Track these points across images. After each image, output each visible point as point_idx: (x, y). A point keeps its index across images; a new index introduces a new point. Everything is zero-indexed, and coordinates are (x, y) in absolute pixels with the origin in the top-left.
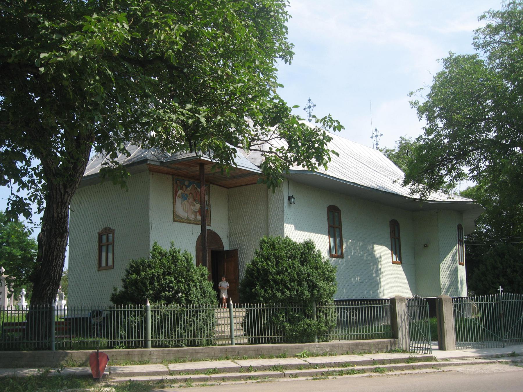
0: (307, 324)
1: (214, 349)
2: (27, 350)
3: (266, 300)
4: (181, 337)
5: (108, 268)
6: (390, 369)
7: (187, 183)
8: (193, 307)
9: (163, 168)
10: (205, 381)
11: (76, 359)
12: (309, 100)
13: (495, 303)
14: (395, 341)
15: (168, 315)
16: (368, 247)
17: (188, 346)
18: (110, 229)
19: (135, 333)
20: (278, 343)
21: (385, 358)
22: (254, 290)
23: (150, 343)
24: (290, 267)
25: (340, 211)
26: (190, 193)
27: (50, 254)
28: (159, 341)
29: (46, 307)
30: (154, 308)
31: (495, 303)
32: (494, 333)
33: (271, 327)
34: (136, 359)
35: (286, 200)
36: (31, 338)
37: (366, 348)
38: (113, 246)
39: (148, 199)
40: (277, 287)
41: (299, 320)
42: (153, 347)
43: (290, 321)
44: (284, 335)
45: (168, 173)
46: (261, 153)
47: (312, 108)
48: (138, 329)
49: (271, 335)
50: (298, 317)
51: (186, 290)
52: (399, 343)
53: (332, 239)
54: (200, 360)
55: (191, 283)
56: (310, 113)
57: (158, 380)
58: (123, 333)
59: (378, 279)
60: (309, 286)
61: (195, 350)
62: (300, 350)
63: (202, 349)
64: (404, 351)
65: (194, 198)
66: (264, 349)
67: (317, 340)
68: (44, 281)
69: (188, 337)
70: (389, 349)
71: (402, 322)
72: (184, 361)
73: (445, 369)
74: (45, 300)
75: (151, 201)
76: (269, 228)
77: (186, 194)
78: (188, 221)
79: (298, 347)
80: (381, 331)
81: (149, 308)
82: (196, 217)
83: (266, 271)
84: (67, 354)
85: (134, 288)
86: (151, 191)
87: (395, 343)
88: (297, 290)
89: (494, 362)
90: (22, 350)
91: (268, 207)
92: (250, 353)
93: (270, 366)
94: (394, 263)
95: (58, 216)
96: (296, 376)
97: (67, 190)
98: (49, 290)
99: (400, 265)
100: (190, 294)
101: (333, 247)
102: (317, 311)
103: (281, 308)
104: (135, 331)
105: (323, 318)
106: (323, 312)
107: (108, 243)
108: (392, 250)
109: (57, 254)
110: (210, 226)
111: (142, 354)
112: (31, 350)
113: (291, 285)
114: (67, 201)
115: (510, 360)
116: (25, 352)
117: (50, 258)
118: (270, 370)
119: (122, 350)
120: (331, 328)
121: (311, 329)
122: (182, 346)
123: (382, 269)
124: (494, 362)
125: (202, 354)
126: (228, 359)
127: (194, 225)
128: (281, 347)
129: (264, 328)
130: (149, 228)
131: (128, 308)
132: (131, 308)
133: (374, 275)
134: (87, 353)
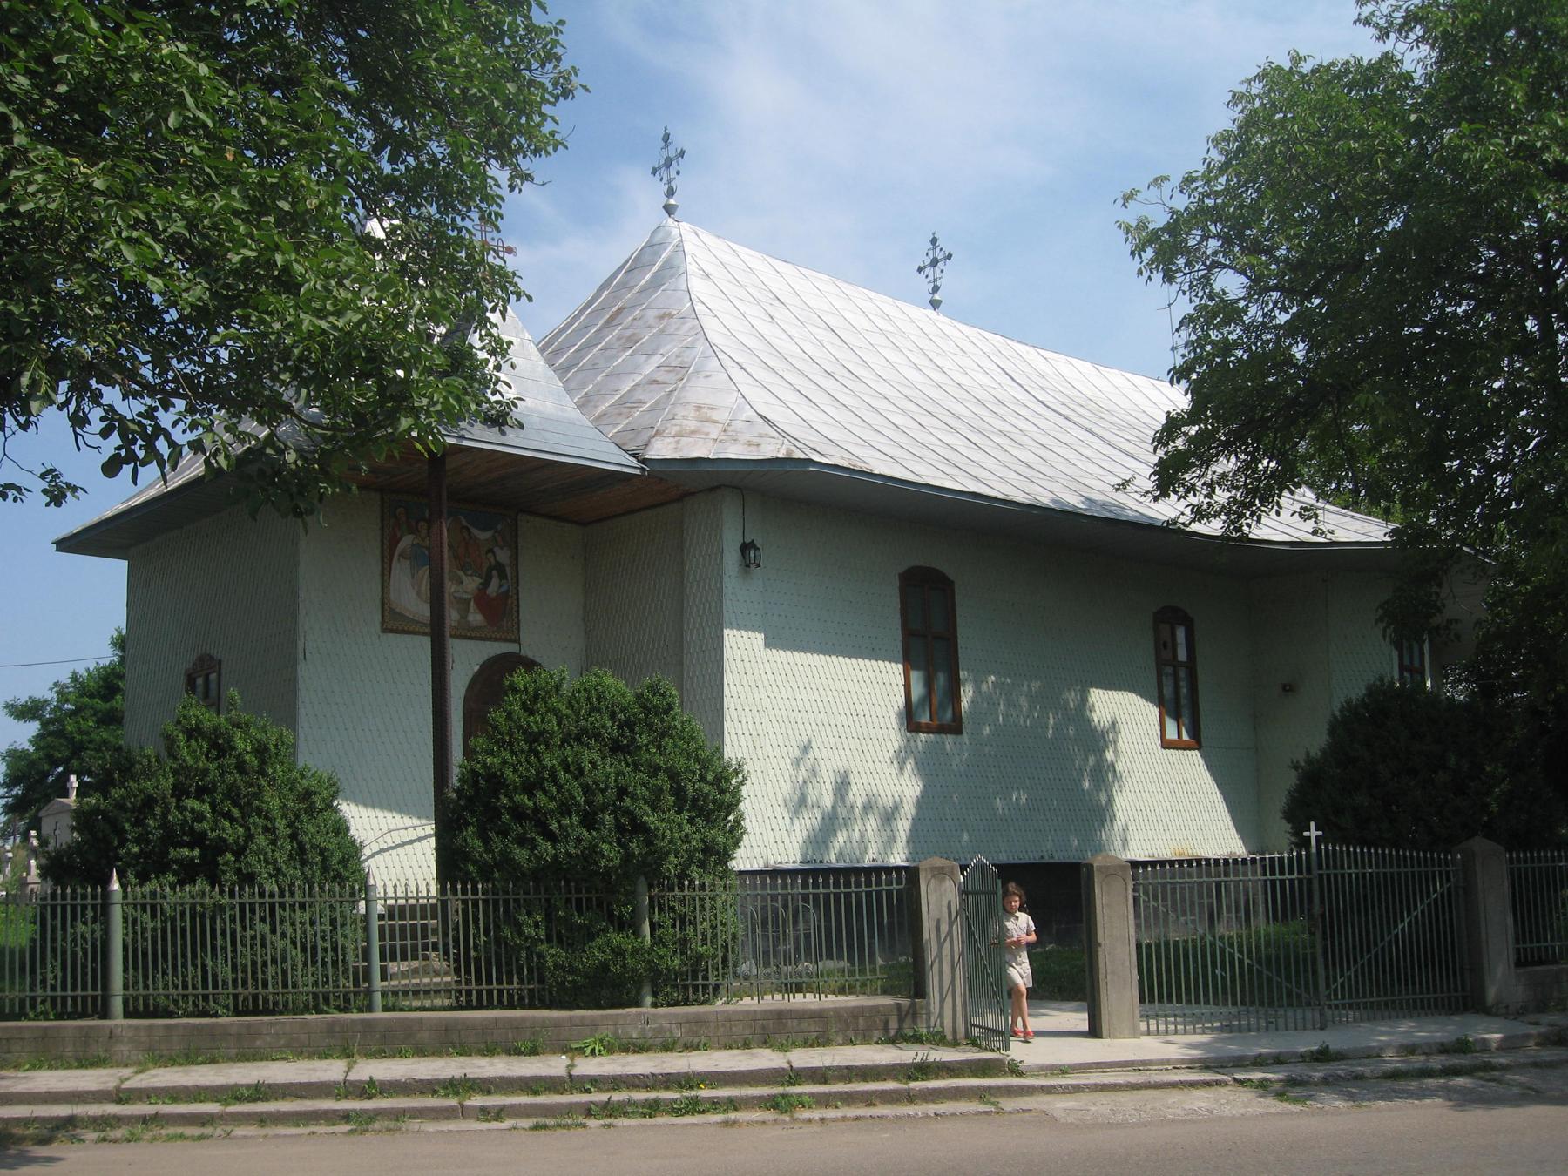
1: (306, 1023)
3: (486, 873)
4: (215, 986)
6: (825, 1101)
8: (262, 895)
10: (203, 1125)
12: (934, 241)
13: (1292, 881)
14: (913, 1005)
15: (173, 920)
16: (1066, 695)
17: (238, 1013)
19: (84, 974)
20: (523, 1007)
21: (827, 1064)
23: (117, 1004)
24: (567, 770)
25: (951, 584)
28: (146, 998)
30: (144, 897)
31: (1292, 881)
32: (1288, 979)
33: (498, 955)
34: (69, 1051)
35: (731, 558)
37: (813, 1029)
42: (128, 1014)
43: (560, 941)
44: (542, 981)
48: (94, 960)
49: (499, 982)
52: (929, 1015)
53: (916, 676)
56: (935, 280)
57: (58, 1118)
59: (1103, 797)
60: (620, 828)
61: (249, 1025)
63: (271, 1024)
67: (649, 1000)
70: (892, 1033)
71: (940, 945)
73: (1008, 1104)
79: (582, 1023)
82: (464, 617)
87: (913, 1013)
89: (1218, 1083)
94: (1166, 744)
96: (499, 1113)
99: (1195, 755)
101: (922, 700)
102: (651, 906)
104: (84, 966)
106: (672, 909)
108: (1160, 703)
110: (518, 641)
111: (87, 1036)
115: (1280, 1076)
118: (434, 1092)
121: (624, 966)
122: (216, 1015)
123: (1120, 766)
124: (1218, 1083)
125: (268, 1039)
128: (523, 1019)
129: (477, 960)
131: (73, 898)
132: (84, 897)
133: (1086, 785)
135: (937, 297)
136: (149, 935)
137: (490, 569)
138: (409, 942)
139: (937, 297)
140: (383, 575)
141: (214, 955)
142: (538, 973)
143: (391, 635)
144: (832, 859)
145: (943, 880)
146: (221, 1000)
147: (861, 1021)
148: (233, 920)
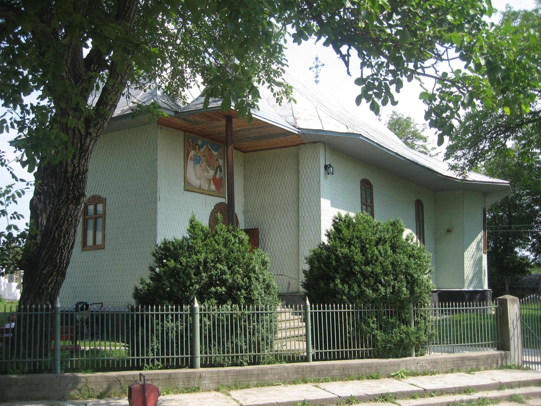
0: (405, 333)
2: (18, 374)
3: (352, 300)
4: (242, 352)
5: (96, 247)
7: (200, 142)
8: (258, 309)
9: (178, 121)
11: (93, 387)
12: (317, 59)
14: (506, 354)
15: (223, 321)
17: (249, 364)
18: (100, 197)
22: (332, 285)
23: (198, 361)
26: (204, 156)
27: (57, 229)
28: (211, 357)
29: (47, 309)
34: (181, 385)
35: (322, 169)
36: (24, 354)
37: (474, 364)
38: (104, 220)
39: (156, 160)
40: (366, 281)
41: (393, 326)
42: (202, 366)
43: (381, 329)
44: (374, 347)
45: (179, 128)
46: (423, 85)
47: (319, 68)
50: (393, 323)
51: (246, 285)
52: (511, 357)
54: (269, 385)
55: (252, 275)
56: (317, 73)
60: (408, 282)
62: (396, 368)
64: (519, 368)
65: (207, 162)
66: (351, 367)
68: (44, 268)
69: (250, 351)
70: (499, 365)
71: (514, 330)
72: (248, 387)
74: (44, 298)
75: (159, 162)
76: (300, 204)
77: (199, 157)
78: (200, 191)
80: (488, 341)
81: (198, 311)
82: (209, 187)
83: (349, 260)
84: (77, 381)
85: (172, 280)
86: (159, 150)
87: (506, 357)
88: (394, 287)
90: (11, 374)
91: (299, 177)
92: (335, 372)
93: (376, 395)
95: (73, 171)
97: (90, 131)
98: (51, 282)
100: (252, 291)
102: (414, 315)
103: (370, 310)
105: (422, 325)
106: (421, 315)
107: (96, 216)
109: (67, 229)
111: (189, 377)
112: (23, 373)
113: (384, 280)
114: (88, 148)
116: (14, 376)
117: (56, 234)
118: (414, 398)
120: (430, 337)
121: (410, 340)
122: (241, 365)
126: (306, 382)
127: (207, 196)
128: (373, 363)
130: (156, 198)
134: (109, 377)
135: (318, 79)
136: (207, 327)
137: (217, 167)
138: (69, 326)
139: (318, 79)
140: (185, 167)
141: (236, 337)
142: (374, 342)
143: (187, 192)
144: (289, 292)
145: (514, 304)
146: (244, 359)
147: (489, 360)
148: (245, 321)
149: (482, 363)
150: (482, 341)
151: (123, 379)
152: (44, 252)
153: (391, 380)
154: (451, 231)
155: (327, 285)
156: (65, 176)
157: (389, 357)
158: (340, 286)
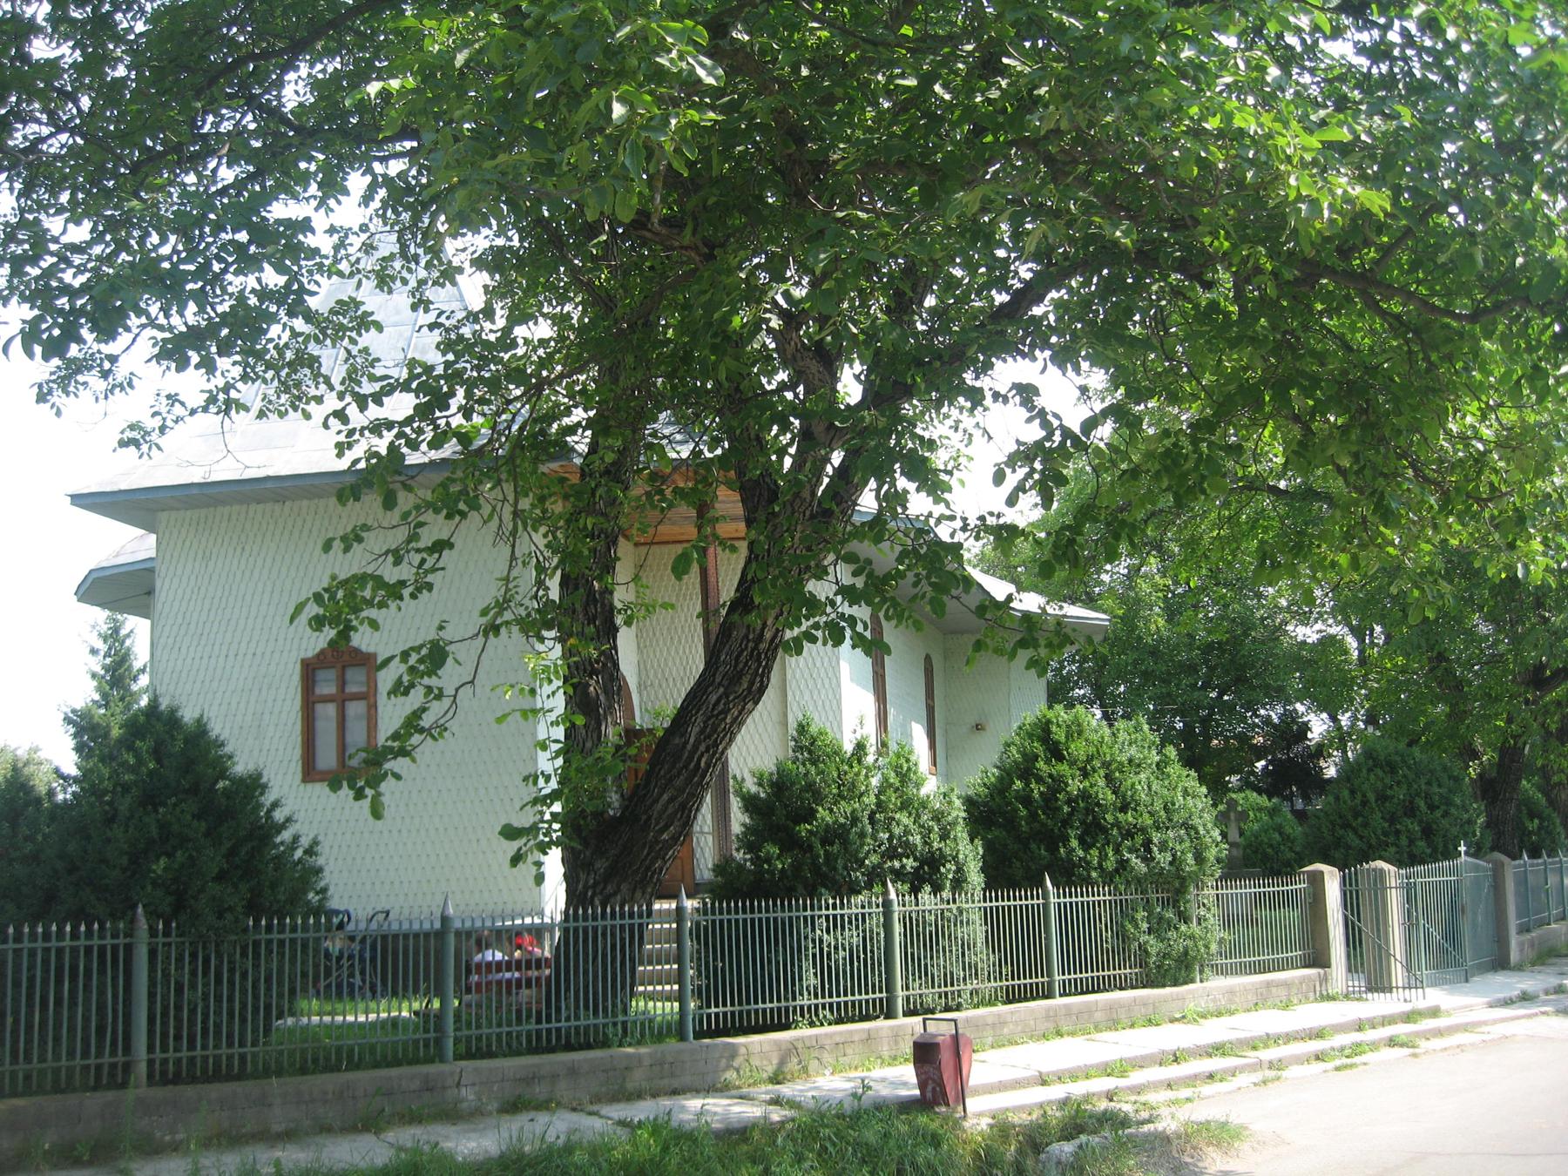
3: (1108, 878)
37: (1283, 992)
42: (905, 1015)
58: (811, 980)
84: (733, 1052)
92: (1098, 1016)
119: (827, 1029)
128: (1149, 997)
149: (1294, 991)
150: (764, 1002)
151: (800, 1046)
152: (665, 797)
153: (1177, 1025)
154: (983, 729)
155: (1053, 850)
156: (756, 647)
157: (1164, 986)
158: (1081, 853)
